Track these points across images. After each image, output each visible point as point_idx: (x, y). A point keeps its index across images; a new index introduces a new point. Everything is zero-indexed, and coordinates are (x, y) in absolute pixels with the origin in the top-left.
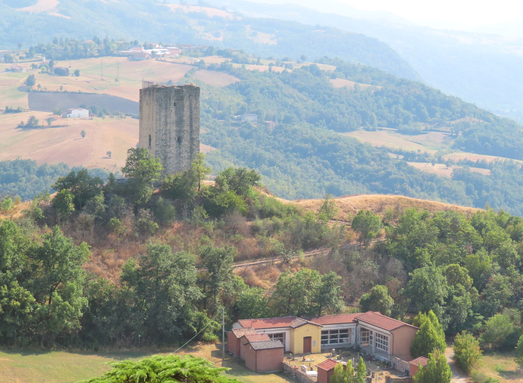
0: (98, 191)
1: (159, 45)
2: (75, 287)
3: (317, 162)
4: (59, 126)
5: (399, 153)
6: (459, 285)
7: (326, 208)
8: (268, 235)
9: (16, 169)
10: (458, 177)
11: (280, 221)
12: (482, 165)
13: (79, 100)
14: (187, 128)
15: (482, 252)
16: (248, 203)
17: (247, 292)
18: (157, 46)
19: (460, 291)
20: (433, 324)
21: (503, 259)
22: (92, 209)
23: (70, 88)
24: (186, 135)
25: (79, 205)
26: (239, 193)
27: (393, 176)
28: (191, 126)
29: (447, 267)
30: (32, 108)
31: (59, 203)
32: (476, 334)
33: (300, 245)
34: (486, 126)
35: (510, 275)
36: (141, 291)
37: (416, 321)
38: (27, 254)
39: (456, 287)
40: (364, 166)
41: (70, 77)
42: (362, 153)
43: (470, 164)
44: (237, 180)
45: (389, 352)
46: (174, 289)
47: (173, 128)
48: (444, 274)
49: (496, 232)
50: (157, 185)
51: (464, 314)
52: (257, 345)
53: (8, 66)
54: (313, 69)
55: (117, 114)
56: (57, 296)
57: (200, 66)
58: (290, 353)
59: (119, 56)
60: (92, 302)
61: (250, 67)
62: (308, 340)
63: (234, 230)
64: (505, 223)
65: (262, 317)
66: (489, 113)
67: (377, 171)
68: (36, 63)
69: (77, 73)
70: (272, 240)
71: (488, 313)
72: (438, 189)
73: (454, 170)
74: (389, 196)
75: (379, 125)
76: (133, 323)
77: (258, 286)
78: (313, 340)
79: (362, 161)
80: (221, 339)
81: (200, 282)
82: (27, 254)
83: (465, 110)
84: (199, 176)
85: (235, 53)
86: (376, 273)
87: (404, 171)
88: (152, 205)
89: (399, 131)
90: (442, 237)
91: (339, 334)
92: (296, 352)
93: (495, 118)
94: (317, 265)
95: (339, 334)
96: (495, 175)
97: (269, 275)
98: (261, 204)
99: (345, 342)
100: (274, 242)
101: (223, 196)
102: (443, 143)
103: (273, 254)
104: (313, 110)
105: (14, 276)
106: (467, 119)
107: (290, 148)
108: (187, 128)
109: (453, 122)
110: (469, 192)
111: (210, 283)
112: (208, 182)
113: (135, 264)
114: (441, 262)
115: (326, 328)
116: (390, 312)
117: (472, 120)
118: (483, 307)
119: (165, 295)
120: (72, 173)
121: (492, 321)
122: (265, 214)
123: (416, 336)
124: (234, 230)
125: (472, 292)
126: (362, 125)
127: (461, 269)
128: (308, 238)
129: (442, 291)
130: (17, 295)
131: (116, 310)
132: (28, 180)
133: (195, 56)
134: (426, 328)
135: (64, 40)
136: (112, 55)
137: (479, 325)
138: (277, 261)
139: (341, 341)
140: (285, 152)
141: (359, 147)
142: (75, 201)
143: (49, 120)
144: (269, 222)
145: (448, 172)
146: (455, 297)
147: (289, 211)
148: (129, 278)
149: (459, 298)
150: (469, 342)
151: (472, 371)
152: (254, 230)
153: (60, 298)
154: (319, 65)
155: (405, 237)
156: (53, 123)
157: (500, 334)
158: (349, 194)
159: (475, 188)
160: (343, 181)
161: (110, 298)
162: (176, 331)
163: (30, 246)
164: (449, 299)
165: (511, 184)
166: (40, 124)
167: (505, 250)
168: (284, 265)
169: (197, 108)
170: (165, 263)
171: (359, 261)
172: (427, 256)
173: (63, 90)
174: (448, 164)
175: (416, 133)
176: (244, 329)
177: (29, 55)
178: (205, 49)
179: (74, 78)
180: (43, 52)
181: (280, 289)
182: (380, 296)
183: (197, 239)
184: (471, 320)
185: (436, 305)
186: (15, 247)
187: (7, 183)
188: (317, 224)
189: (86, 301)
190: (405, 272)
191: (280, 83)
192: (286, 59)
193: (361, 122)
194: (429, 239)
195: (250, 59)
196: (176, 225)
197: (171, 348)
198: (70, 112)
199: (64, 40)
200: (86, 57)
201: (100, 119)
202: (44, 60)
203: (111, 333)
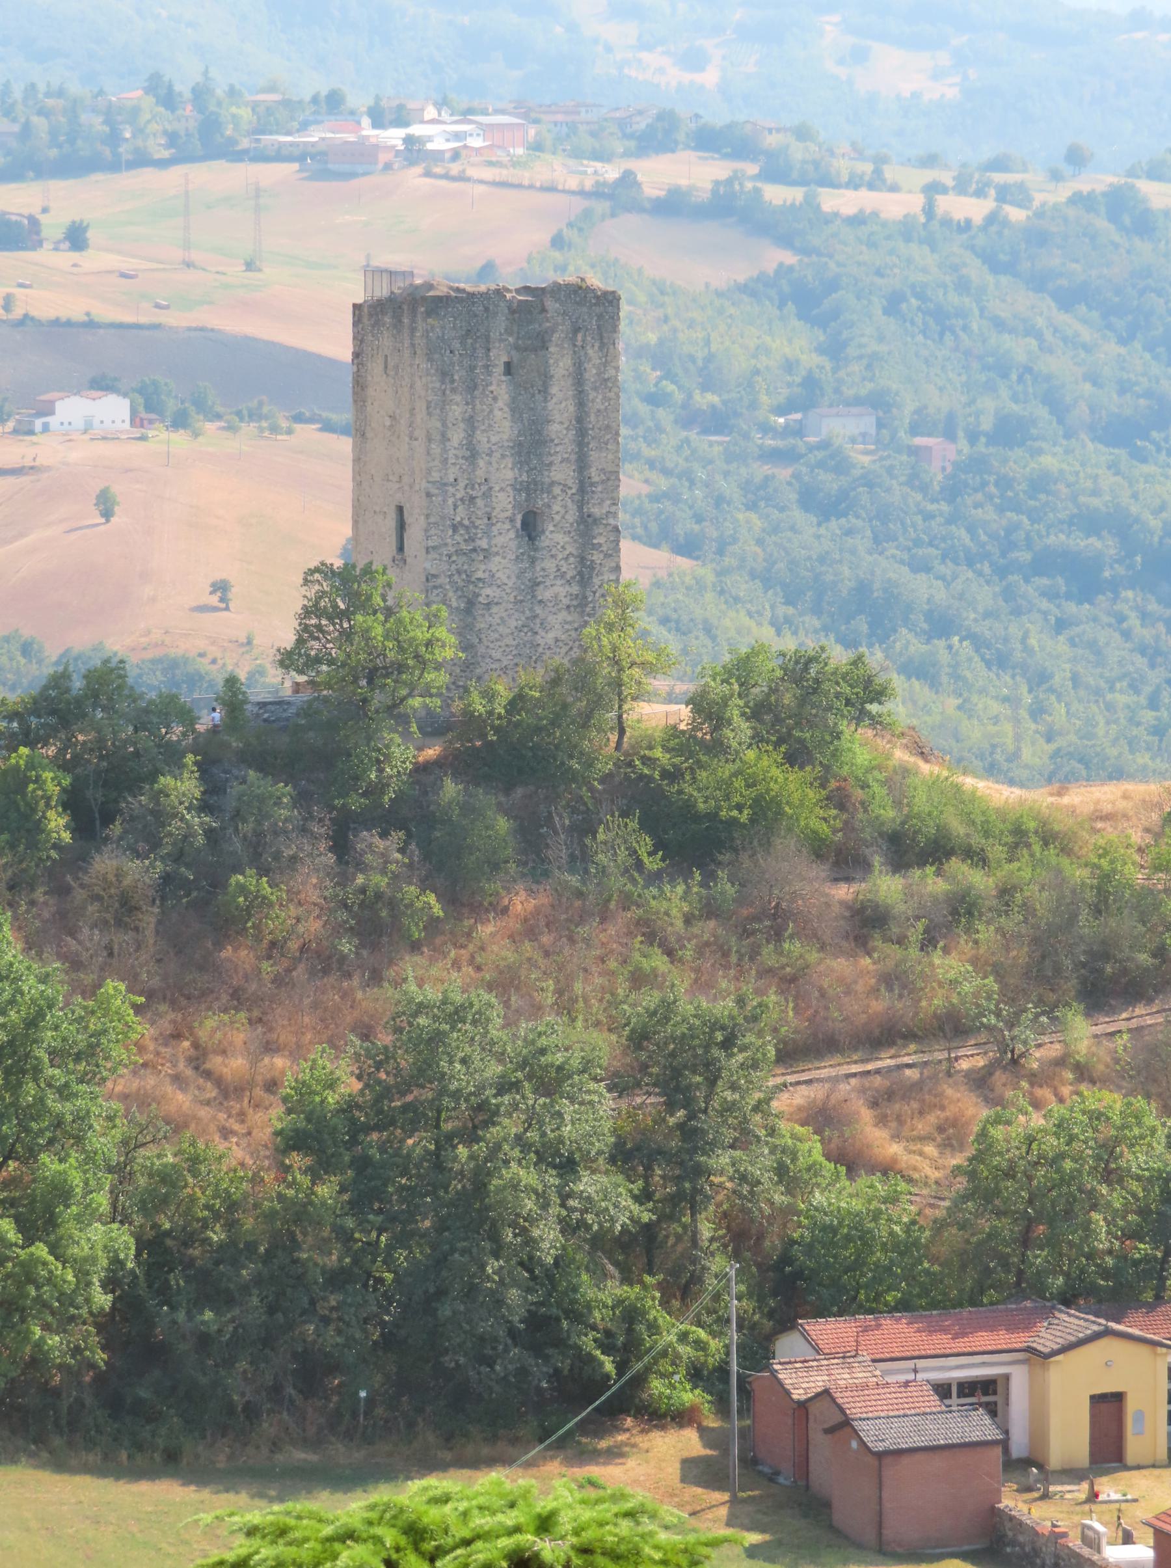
0: (172, 757)
1: (439, 106)
2: (76, 1179)
3: (1145, 617)
8: (929, 942)
11: (980, 881)
14: (562, 473)
16: (839, 800)
17: (838, 1197)
18: (431, 112)
22: (148, 834)
23: (46, 304)
24: (561, 504)
26: (796, 757)
28: (582, 463)
33: (1071, 985)
41: (44, 256)
50: (434, 727)
54: (1119, 204)
57: (620, 196)
58: (1029, 1467)
59: (262, 157)
60: (152, 1246)
61: (839, 202)
62: (1108, 1408)
63: (777, 922)
65: (904, 1306)
69: (76, 238)
70: (949, 965)
77: (886, 1169)
78: (1131, 1406)
80: (722, 1406)
81: (628, 1155)
85: (772, 141)
88: (412, 815)
92: (1055, 1460)
97: (932, 1118)
98: (897, 804)
103: (953, 1027)
108: (562, 473)
112: (658, 712)
119: (475, 1213)
122: (913, 848)
124: (777, 922)
128: (1106, 956)
131: (258, 1280)
136: (233, 154)
138: (970, 1060)
140: (1002, 572)
142: (72, 802)
144: (933, 883)
148: (313, 1137)
152: (867, 923)
168: (999, 1077)
169: (608, 383)
170: (471, 1069)
173: (18, 312)
176: (817, 1363)
178: (641, 124)
179: (66, 259)
181: (984, 1184)
183: (612, 964)
189: (124, 1240)
191: (975, 270)
192: (999, 164)
195: (842, 166)
196: (521, 902)
198: (47, 410)
200: (115, 166)
201: (179, 440)
203: (239, 1382)
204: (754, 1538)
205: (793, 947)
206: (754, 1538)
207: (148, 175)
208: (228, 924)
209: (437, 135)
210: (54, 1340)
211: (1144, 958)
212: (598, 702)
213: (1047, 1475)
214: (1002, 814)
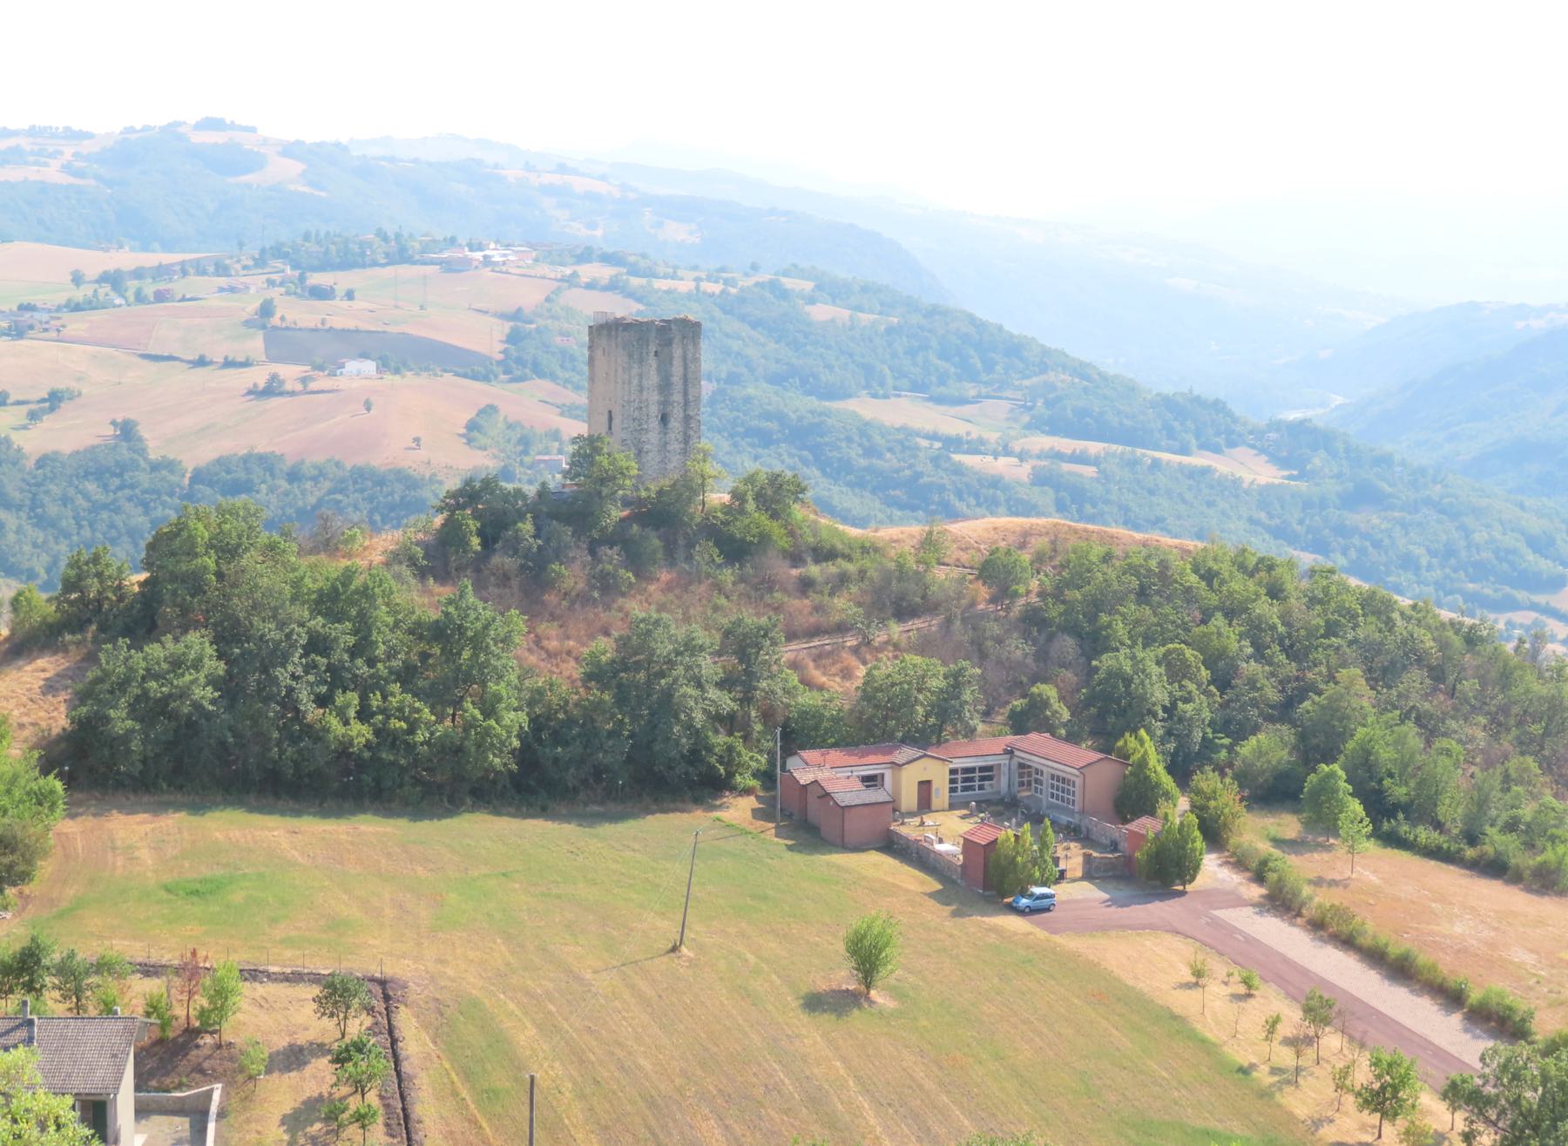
0: (521, 516)
1: (497, 242)
2: (504, 694)
3: (790, 455)
4: (322, 392)
5: (933, 437)
6: (1186, 682)
7: (928, 543)
8: (832, 594)
9: (248, 470)
10: (1040, 479)
11: (851, 568)
14: (677, 397)
16: (792, 534)
17: (807, 699)
18: (492, 245)
19: (1190, 693)
20: (1147, 749)
21: (1256, 633)
22: (514, 547)
23: (339, 322)
24: (676, 409)
25: (488, 542)
26: (774, 516)
27: (926, 479)
28: (686, 393)
29: (1162, 650)
30: (272, 359)
31: (450, 537)
32: (1220, 770)
33: (890, 611)
34: (1085, 389)
35: (1270, 664)
36: (621, 700)
37: (1120, 749)
38: (411, 632)
39: (1181, 687)
40: (874, 461)
41: (336, 302)
42: (869, 438)
43: (1058, 456)
44: (769, 492)
45: (1077, 808)
46: (684, 695)
47: (654, 397)
48: (1158, 663)
49: (1239, 585)
50: (626, 503)
51: (1197, 736)
53: (223, 281)
54: (774, 286)
55: (427, 369)
56: (472, 710)
57: (571, 281)
59: (425, 264)
60: (534, 720)
61: (661, 284)
62: (925, 786)
63: (769, 585)
64: (1251, 567)
65: (835, 745)
66: (1088, 365)
67: (897, 471)
68: (273, 277)
69: (350, 295)
70: (840, 602)
71: (1241, 732)
72: (1008, 501)
73: (1033, 468)
74: (1034, 520)
75: (895, 388)
76: (609, 759)
77: (821, 688)
78: (934, 786)
79: (870, 452)
80: (765, 788)
82: (411, 632)
83: (1047, 360)
84: (703, 485)
85: (632, 259)
86: (1029, 661)
87: (945, 470)
88: (618, 538)
89: (930, 399)
90: (1143, 595)
91: (977, 774)
92: (904, 808)
93: (1099, 374)
94: (924, 646)
95: (977, 774)
96: (1105, 477)
97: (838, 666)
98: (814, 536)
99: (988, 789)
100: (842, 605)
101: (747, 521)
102: (1008, 419)
103: (841, 628)
104: (778, 361)
105: (391, 673)
106: (1051, 376)
107: (741, 429)
108: (677, 397)
109: (1026, 383)
111: (743, 683)
112: (718, 497)
113: (605, 648)
115: (959, 764)
116: (1063, 732)
117: (1060, 379)
118: (1227, 722)
119: (667, 705)
120: (469, 482)
121: (1247, 749)
122: (824, 554)
123: (1125, 777)
124: (769, 585)
125: (1206, 693)
126: (864, 388)
127: (1189, 653)
128: (902, 599)
129: (1159, 694)
130: (400, 710)
131: (579, 735)
132: (271, 490)
133: (562, 264)
134: (1143, 763)
135: (322, 234)
137: (1223, 754)
138: (851, 642)
139: (981, 788)
140: (732, 436)
141: (865, 428)
142: (480, 533)
143: (304, 380)
144: (832, 568)
145: (1024, 472)
146: (1180, 704)
147: (865, 550)
148: (597, 675)
149: (1189, 707)
150: (1225, 794)
151: (1231, 841)
152: (806, 585)
153: (477, 713)
154: (784, 280)
155: (1078, 595)
156: (313, 386)
157: (1264, 772)
158: (966, 518)
159: (1072, 497)
160: (836, 489)
161: (566, 712)
162: (686, 773)
163: (414, 617)
164: (1170, 710)
165: (1135, 493)
166: (288, 387)
167: (1259, 617)
168: (863, 649)
169: (696, 360)
171: (999, 641)
172: (1120, 629)
173: (327, 326)
174: (1022, 457)
175: (962, 401)
176: (808, 769)
177: (260, 262)
178: (579, 251)
179: (346, 303)
180: (285, 256)
181: (869, 693)
182: (1046, 704)
183: (704, 602)
185: (1148, 719)
186: (390, 620)
187: (233, 495)
188: (917, 573)
189: (523, 718)
190: (1082, 660)
191: (718, 313)
192: (723, 270)
193: (863, 382)
194: (1121, 599)
195: (661, 270)
196: (665, 576)
197: (680, 805)
198: (342, 366)
199: (322, 234)
200: (364, 266)
201: (397, 378)
202: (289, 271)
203: (571, 777)
204: (790, 842)
205: (777, 595)
206: (790, 842)
207: (377, 269)
210: (497, 760)
211: (918, 600)
212: (695, 492)
213: (903, 815)
214: (856, 539)
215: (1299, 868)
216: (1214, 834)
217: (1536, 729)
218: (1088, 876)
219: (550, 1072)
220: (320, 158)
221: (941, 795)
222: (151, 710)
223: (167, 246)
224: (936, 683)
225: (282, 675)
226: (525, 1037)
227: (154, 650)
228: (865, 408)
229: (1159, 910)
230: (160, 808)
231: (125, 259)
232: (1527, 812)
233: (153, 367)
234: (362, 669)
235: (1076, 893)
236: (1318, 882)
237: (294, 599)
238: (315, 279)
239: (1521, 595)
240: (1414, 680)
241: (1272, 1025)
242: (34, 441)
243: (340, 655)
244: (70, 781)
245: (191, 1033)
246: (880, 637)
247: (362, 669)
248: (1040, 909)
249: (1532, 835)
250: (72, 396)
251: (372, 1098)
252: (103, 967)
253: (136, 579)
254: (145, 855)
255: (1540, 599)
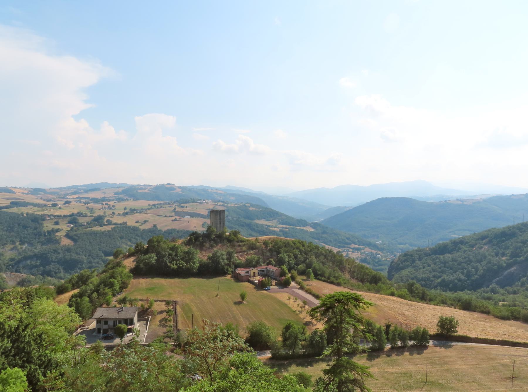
10: (281, 231)
12: (286, 228)
13: (187, 214)
15: (295, 250)
17: (239, 261)
20: (285, 268)
21: (301, 251)
25: (196, 240)
31: (190, 240)
32: (295, 270)
43: (283, 228)
47: (219, 220)
49: (298, 245)
52: (242, 275)
54: (244, 205)
57: (217, 205)
58: (250, 276)
62: (254, 273)
71: (298, 265)
79: (257, 227)
81: (227, 259)
83: (282, 215)
88: (214, 240)
90: (285, 246)
94: (255, 254)
96: (289, 230)
100: (244, 248)
103: (244, 251)
110: (283, 234)
112: (227, 234)
113: (211, 255)
114: (286, 252)
117: (284, 217)
119: (219, 262)
122: (242, 241)
129: (287, 260)
148: (209, 258)
150: (295, 272)
152: (239, 246)
159: (285, 234)
164: (288, 262)
170: (218, 254)
172: (282, 251)
174: (278, 228)
177: (174, 203)
181: (247, 260)
184: (294, 267)
196: (220, 245)
208: (203, 246)
209: (207, 201)
215: (305, 284)
216: (293, 278)
217: (338, 264)
218: (276, 285)
219: (197, 314)
220: (183, 188)
221: (257, 274)
222: (146, 264)
223: (162, 200)
224: (256, 259)
225: (165, 259)
226: (194, 309)
227: (147, 256)
228: (257, 222)
229: (285, 289)
230: (147, 278)
231: (156, 202)
232: (336, 275)
233: (159, 217)
234: (176, 258)
235: (274, 287)
236: (307, 285)
237: (167, 248)
238: (182, 205)
239: (346, 246)
240: (322, 257)
241: (298, 305)
242: (142, 227)
243: (173, 256)
244: (134, 275)
245: (147, 309)
246: (249, 253)
247: (176, 258)
248: (269, 289)
249: (337, 278)
250: (148, 221)
251: (172, 318)
252: (135, 300)
253: (146, 246)
254: (144, 284)
255: (349, 246)
